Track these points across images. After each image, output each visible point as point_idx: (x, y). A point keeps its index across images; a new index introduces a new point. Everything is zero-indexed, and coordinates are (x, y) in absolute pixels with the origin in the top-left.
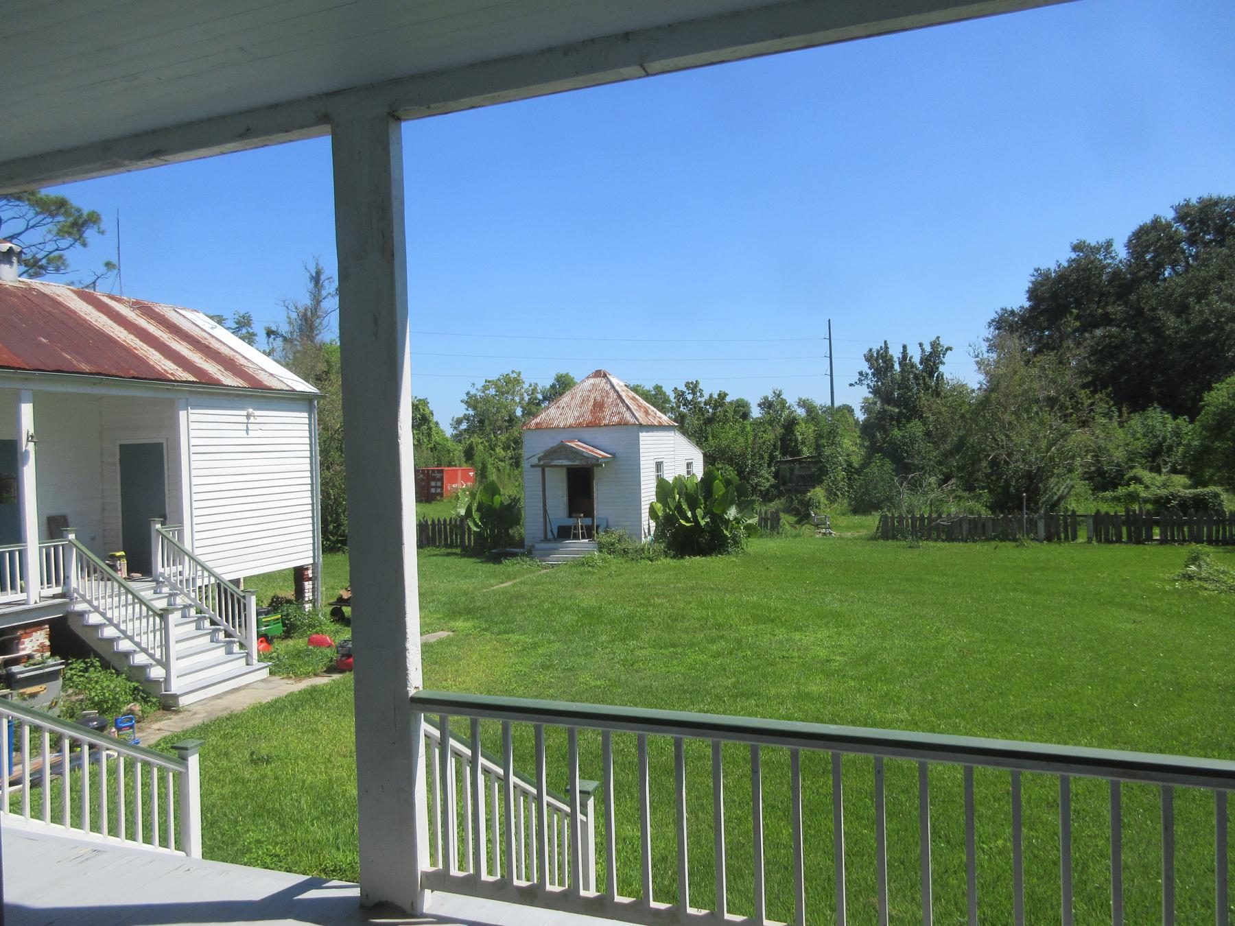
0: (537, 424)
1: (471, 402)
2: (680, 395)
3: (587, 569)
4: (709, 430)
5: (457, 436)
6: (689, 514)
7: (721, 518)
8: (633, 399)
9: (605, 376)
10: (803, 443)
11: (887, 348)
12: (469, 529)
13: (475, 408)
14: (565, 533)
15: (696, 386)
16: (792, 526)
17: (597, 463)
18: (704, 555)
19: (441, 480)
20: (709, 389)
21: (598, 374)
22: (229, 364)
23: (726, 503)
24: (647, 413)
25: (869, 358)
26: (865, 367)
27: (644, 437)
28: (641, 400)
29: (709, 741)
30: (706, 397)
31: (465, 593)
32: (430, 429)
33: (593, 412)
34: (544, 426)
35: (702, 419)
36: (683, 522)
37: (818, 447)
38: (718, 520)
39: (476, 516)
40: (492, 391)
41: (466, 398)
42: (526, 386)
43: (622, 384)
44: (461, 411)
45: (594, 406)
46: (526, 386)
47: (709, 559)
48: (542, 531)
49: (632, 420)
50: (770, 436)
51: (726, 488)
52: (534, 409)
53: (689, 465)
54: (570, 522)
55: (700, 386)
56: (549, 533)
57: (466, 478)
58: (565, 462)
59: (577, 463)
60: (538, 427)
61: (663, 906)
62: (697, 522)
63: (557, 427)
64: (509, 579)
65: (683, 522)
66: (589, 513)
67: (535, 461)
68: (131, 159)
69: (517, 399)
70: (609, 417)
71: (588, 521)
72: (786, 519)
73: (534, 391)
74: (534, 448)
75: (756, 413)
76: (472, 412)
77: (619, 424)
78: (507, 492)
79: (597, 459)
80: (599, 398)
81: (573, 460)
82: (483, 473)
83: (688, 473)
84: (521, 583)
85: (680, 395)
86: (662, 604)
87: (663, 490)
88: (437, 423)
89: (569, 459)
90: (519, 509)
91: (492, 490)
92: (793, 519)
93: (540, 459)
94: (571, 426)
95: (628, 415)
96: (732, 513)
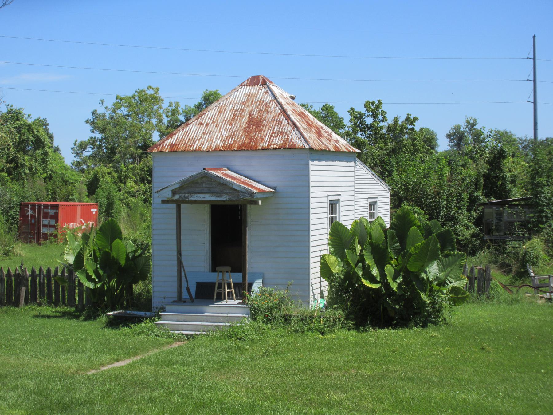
0: (172, 145)
1: (97, 122)
2: (358, 118)
3: (234, 342)
4: (393, 161)
5: (78, 164)
6: (375, 272)
7: (417, 276)
8: (301, 115)
9: (264, 83)
10: (513, 182)
12: (81, 284)
13: (103, 131)
14: (207, 293)
15: (377, 107)
16: (505, 287)
17: (251, 199)
18: (395, 327)
19: (55, 217)
20: (394, 112)
21: (255, 81)
22: (256, 188)
23: (428, 256)
24: (319, 134)
27: (317, 169)
28: (312, 118)
30: (390, 120)
31: (63, 377)
32: (46, 154)
33: (247, 130)
34: (182, 147)
35: (385, 146)
36: (367, 283)
37: (535, 186)
38: (413, 281)
39: (90, 267)
40: (124, 111)
41: (91, 117)
42: (165, 105)
43: (287, 95)
44: (86, 133)
45: (249, 123)
46: (165, 105)
47: (401, 332)
48: (176, 290)
49: (300, 143)
50: (472, 171)
51: (426, 237)
52: (171, 130)
53: (372, 205)
54: (214, 278)
55: (384, 108)
56: (185, 295)
57: (87, 216)
58: (208, 197)
59: (224, 198)
60: (174, 150)
62: (387, 286)
63: (199, 151)
64: (128, 354)
65: (367, 283)
66: (239, 266)
67: (167, 194)
68: (373, 256)
69: (154, 121)
70: (268, 138)
71: (237, 277)
72: (498, 278)
73: (175, 112)
74: (169, 176)
75: (443, 145)
76: (98, 135)
77: (282, 148)
78: (130, 237)
79: (252, 194)
80: (255, 113)
81: (219, 194)
82: (109, 209)
83: (371, 215)
84: (143, 361)
85: (358, 118)
86: (340, 403)
87: (340, 238)
88: (57, 150)
89: (213, 193)
90: (148, 259)
91: (111, 232)
92: (505, 279)
93: (174, 192)
94: (217, 150)
95: (294, 137)
96: (433, 270)
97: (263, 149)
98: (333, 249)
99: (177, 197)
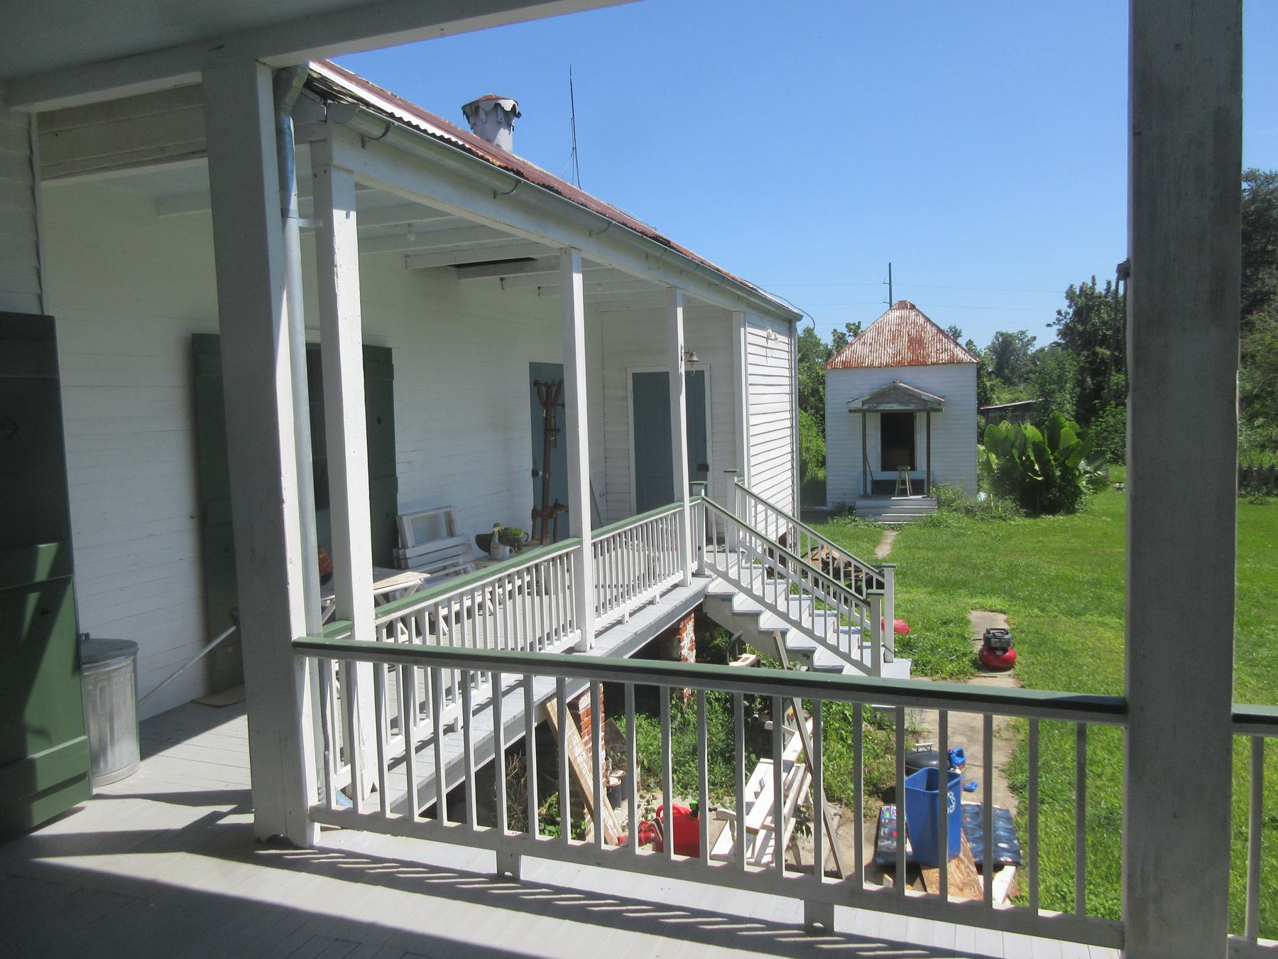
11: (1094, 284)
14: (883, 489)
15: (859, 327)
25: (1070, 295)
26: (1064, 305)
29: (1071, 724)
60: (846, 366)
61: (546, 838)
80: (913, 333)
81: (907, 403)
89: (901, 403)
97: (933, 364)
98: (1093, 419)
99: (866, 407)
